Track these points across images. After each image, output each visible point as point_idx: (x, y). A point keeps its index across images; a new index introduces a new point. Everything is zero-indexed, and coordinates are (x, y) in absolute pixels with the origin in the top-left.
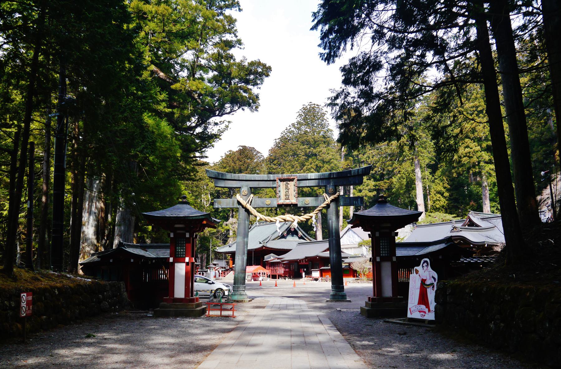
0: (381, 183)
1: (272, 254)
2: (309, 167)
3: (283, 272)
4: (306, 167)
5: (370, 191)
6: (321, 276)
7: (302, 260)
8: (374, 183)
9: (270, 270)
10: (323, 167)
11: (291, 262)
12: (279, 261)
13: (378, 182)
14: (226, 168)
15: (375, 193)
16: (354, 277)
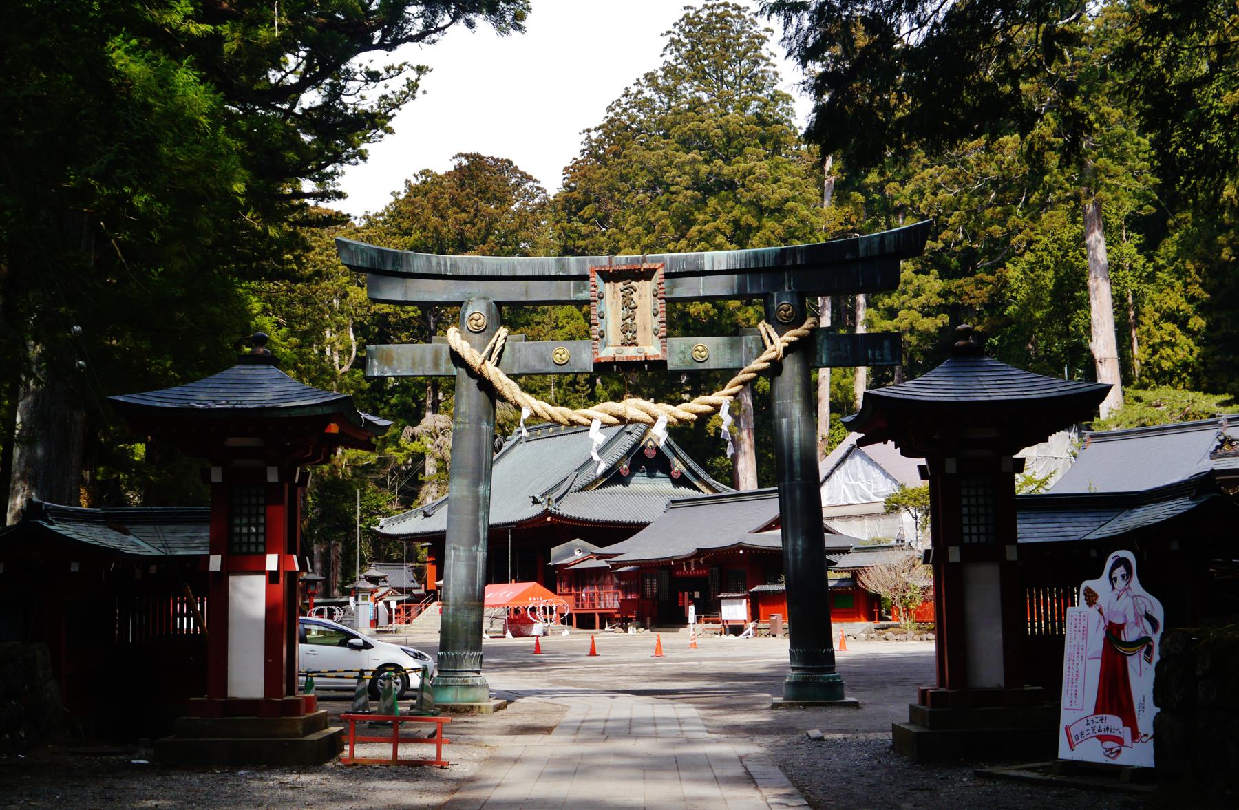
0: (966, 284)
1: (578, 542)
3: (617, 605)
4: (697, 227)
5: (927, 312)
6: (755, 615)
7: (687, 560)
8: (938, 285)
9: (572, 598)
10: (758, 229)
11: (647, 568)
12: (602, 563)
15: (943, 319)
16: (871, 618)
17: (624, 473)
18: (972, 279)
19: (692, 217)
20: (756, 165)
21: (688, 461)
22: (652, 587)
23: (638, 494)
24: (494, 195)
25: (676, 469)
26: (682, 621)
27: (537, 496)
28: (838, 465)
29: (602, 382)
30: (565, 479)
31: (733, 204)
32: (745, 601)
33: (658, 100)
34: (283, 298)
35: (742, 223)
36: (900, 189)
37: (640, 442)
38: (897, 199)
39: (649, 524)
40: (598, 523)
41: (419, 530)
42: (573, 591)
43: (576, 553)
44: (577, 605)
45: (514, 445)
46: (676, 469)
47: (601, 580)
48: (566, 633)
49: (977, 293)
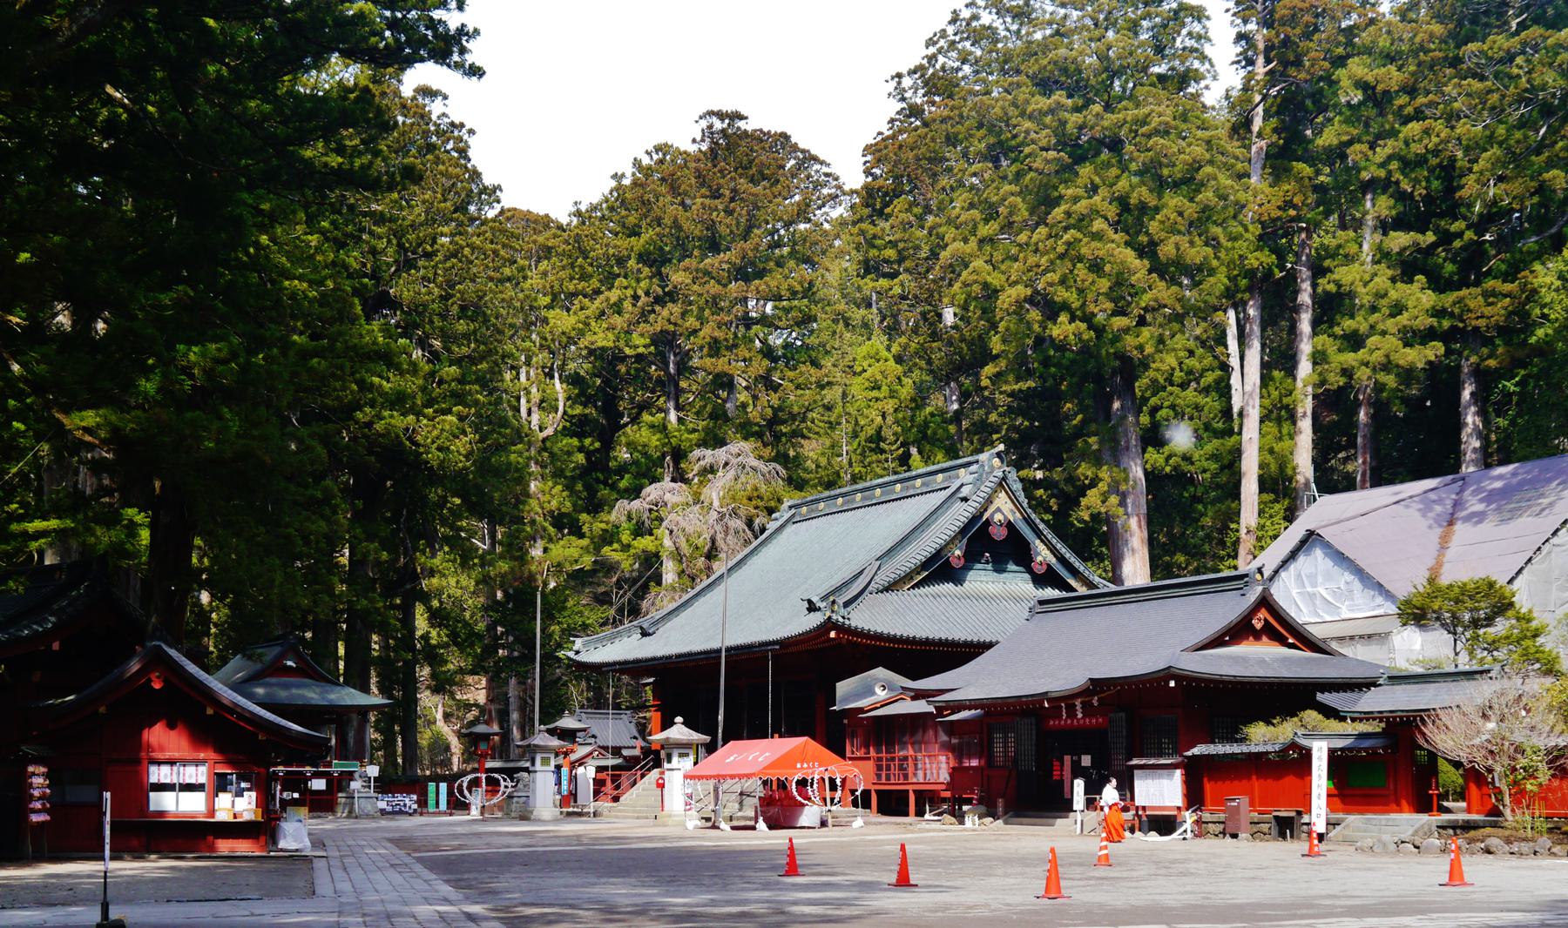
0: (1472, 297)
1: (880, 672)
2: (1082, 206)
3: (944, 776)
4: (1063, 207)
5: (1412, 337)
6: (1194, 797)
7: (1068, 699)
8: (1428, 299)
9: (870, 765)
10: (1157, 210)
12: (921, 707)
13: (1455, 295)
14: (638, 234)
15: (1434, 350)
16: (1423, 804)
17: (957, 564)
18: (1479, 290)
19: (1056, 194)
20: (1153, 111)
21: (1059, 546)
22: (1005, 747)
23: (979, 597)
24: (761, 172)
25: (1039, 559)
26: (1066, 807)
27: (815, 599)
28: (1285, 563)
29: (920, 452)
30: (861, 573)
31: (1119, 172)
32: (1178, 773)
33: (1002, 27)
34: (435, 306)
35: (1132, 201)
36: (1370, 153)
37: (982, 514)
38: (1365, 168)
39: (997, 643)
40: (913, 641)
41: (631, 656)
42: (873, 753)
43: (878, 690)
44: (879, 776)
45: (782, 526)
46: (1039, 559)
47: (919, 736)
48: (858, 823)
49: (1488, 311)
